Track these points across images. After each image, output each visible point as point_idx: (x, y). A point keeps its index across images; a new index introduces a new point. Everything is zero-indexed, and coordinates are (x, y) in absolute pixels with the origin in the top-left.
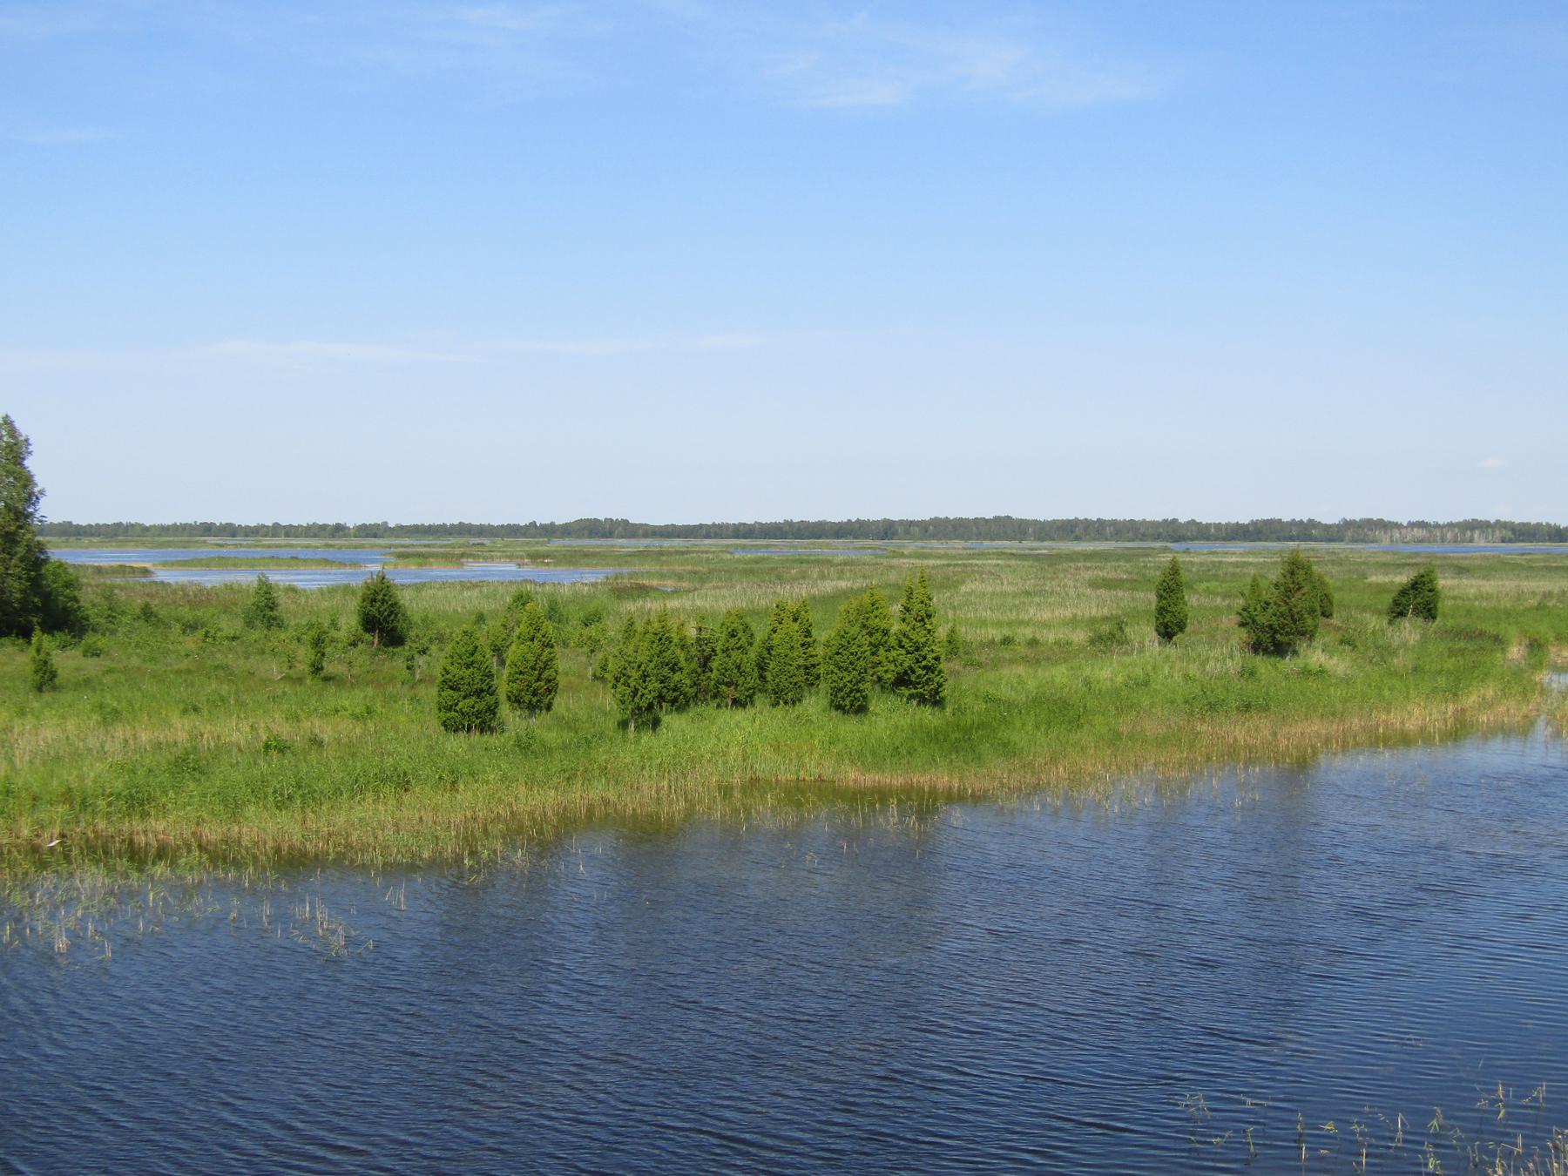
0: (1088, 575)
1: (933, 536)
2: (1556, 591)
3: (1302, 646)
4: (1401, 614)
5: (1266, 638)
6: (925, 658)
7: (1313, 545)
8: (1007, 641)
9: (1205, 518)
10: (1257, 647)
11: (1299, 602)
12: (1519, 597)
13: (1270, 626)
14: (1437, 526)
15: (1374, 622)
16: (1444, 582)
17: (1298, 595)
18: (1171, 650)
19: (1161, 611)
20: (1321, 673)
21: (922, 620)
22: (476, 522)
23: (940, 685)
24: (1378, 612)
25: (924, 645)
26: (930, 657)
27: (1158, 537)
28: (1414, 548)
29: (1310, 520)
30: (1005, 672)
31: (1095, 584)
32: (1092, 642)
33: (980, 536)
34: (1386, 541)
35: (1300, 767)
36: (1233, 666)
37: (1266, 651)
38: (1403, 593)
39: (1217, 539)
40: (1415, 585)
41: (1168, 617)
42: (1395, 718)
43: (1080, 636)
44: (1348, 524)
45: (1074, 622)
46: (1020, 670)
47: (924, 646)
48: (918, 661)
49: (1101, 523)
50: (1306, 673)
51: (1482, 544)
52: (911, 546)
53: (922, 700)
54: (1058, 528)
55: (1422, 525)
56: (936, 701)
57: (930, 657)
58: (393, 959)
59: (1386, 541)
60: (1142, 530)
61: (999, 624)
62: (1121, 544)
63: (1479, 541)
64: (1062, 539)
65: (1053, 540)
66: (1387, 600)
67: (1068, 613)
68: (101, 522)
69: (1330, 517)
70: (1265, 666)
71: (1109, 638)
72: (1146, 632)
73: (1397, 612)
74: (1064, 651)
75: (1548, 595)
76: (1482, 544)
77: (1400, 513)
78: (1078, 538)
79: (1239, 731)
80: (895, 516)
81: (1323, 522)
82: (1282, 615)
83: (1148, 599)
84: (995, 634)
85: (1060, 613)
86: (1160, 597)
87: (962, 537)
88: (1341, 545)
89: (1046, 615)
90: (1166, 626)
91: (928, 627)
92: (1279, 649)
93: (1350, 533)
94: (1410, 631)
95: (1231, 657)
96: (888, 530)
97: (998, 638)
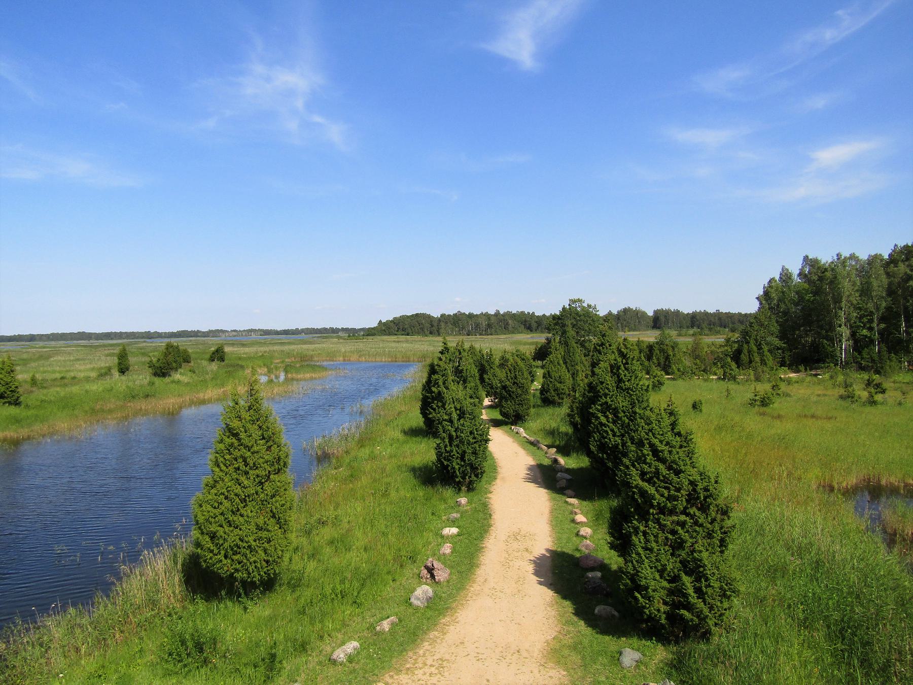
0: (106, 352)
1: (52, 340)
2: (268, 350)
3: (172, 373)
4: (213, 360)
5: (158, 372)
6: (11, 387)
7: (198, 338)
8: (62, 378)
9: (161, 330)
10: (155, 374)
11: (170, 358)
12: (257, 353)
13: (160, 367)
14: (240, 331)
15: (205, 363)
16: (227, 349)
17: (170, 356)
18: (123, 378)
19: (120, 364)
20: (178, 382)
21: (9, 373)
22: (687, 309)
23: (18, 397)
24: (206, 360)
25: (10, 382)
26: (13, 387)
27: (143, 337)
28: (233, 338)
29: (198, 331)
30: (51, 390)
31: (107, 355)
32: (99, 376)
33: (72, 339)
34: (224, 336)
35: (172, 416)
36: (146, 381)
37: (159, 376)
38: (213, 353)
39: (165, 337)
40: (217, 351)
41: (122, 366)
42: (201, 395)
43: (93, 374)
44: (211, 331)
45: (93, 369)
46: (58, 389)
47: (10, 382)
48: (8, 389)
49: (63, 334)
50: (173, 382)
51: (254, 336)
52: (41, 344)
53: (10, 403)
54: (105, 336)
55: (235, 331)
56: (17, 403)
57: (13, 387)
58: (398, 342)
59: (224, 336)
60: (137, 335)
61: (59, 372)
62: (129, 340)
63: (253, 336)
64: (106, 339)
65: (102, 340)
66: (208, 356)
67: (92, 366)
68: (724, 310)
69: (204, 329)
70: (157, 380)
71: (105, 373)
72: (116, 374)
73: (212, 360)
74: (87, 379)
75: (265, 352)
76: (254, 336)
77: (229, 328)
78: (112, 339)
79: (143, 405)
80: (35, 333)
81: (548, 314)
82: (164, 363)
83: (116, 360)
84: (58, 376)
85: (89, 366)
86: (119, 359)
87: (64, 340)
88: (208, 338)
89: (82, 368)
90: (122, 369)
91: (12, 375)
92: (164, 375)
93: (211, 334)
94: (214, 366)
95: (146, 378)
96: (32, 338)
97: (59, 377)
